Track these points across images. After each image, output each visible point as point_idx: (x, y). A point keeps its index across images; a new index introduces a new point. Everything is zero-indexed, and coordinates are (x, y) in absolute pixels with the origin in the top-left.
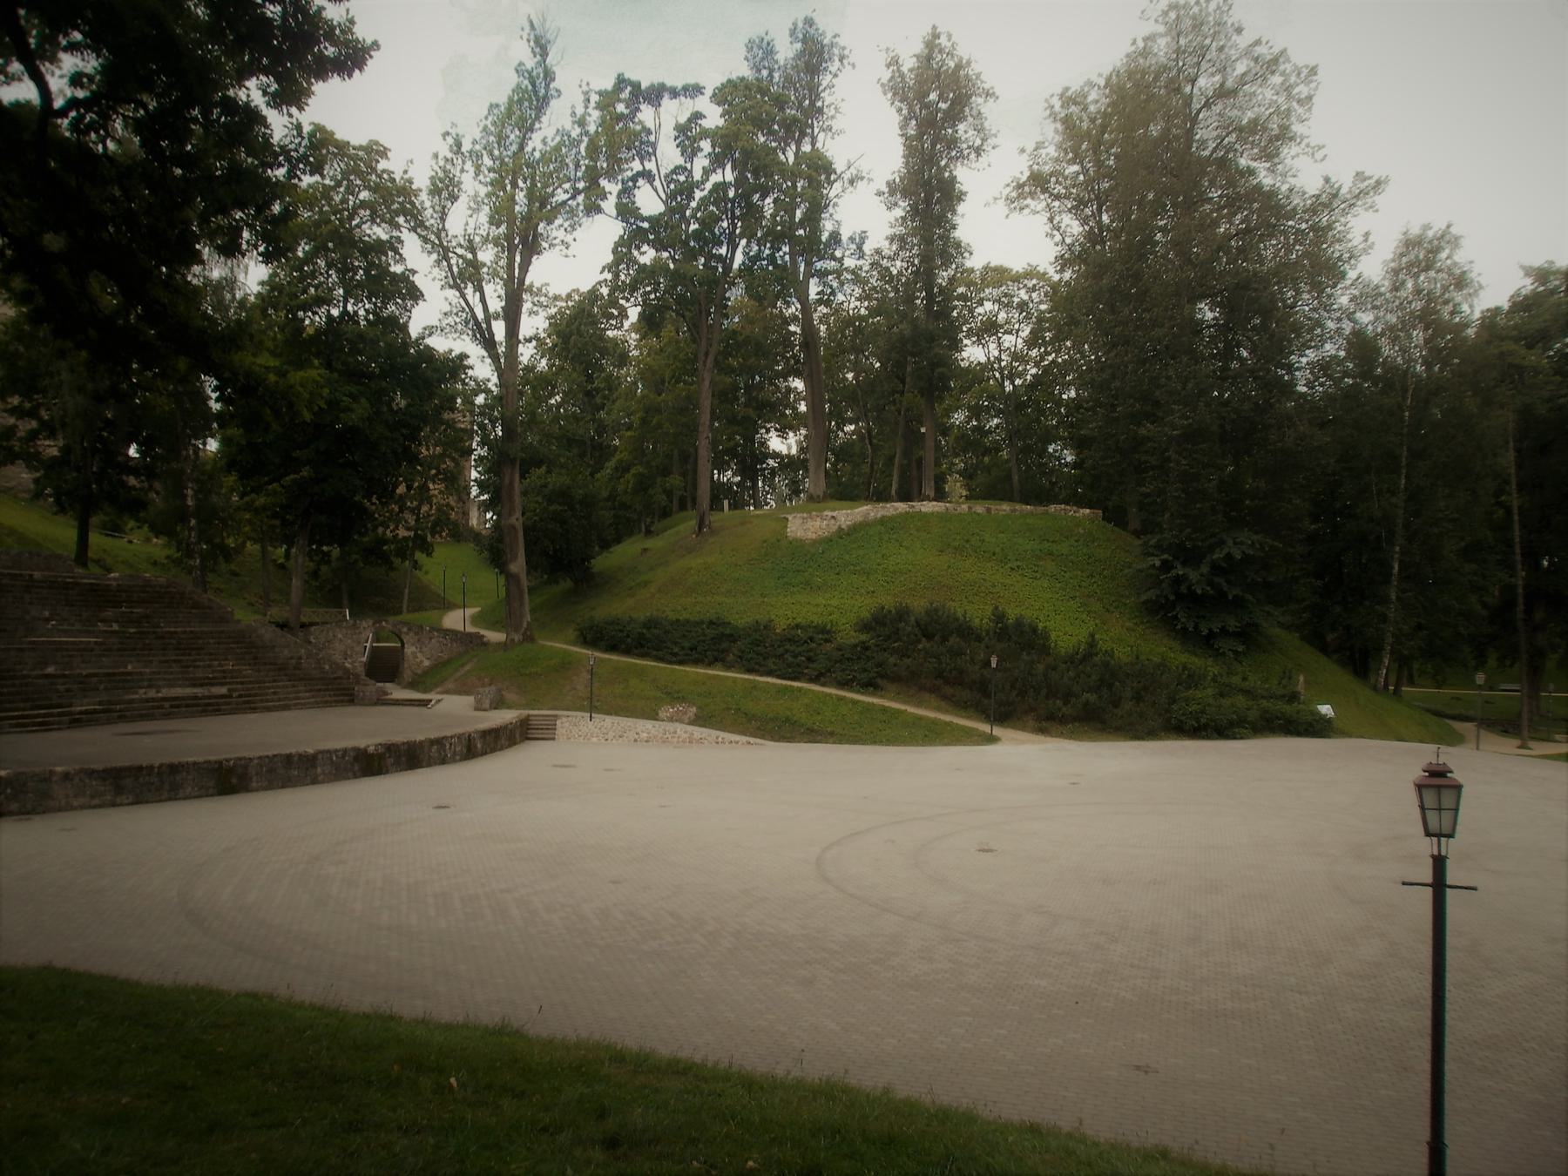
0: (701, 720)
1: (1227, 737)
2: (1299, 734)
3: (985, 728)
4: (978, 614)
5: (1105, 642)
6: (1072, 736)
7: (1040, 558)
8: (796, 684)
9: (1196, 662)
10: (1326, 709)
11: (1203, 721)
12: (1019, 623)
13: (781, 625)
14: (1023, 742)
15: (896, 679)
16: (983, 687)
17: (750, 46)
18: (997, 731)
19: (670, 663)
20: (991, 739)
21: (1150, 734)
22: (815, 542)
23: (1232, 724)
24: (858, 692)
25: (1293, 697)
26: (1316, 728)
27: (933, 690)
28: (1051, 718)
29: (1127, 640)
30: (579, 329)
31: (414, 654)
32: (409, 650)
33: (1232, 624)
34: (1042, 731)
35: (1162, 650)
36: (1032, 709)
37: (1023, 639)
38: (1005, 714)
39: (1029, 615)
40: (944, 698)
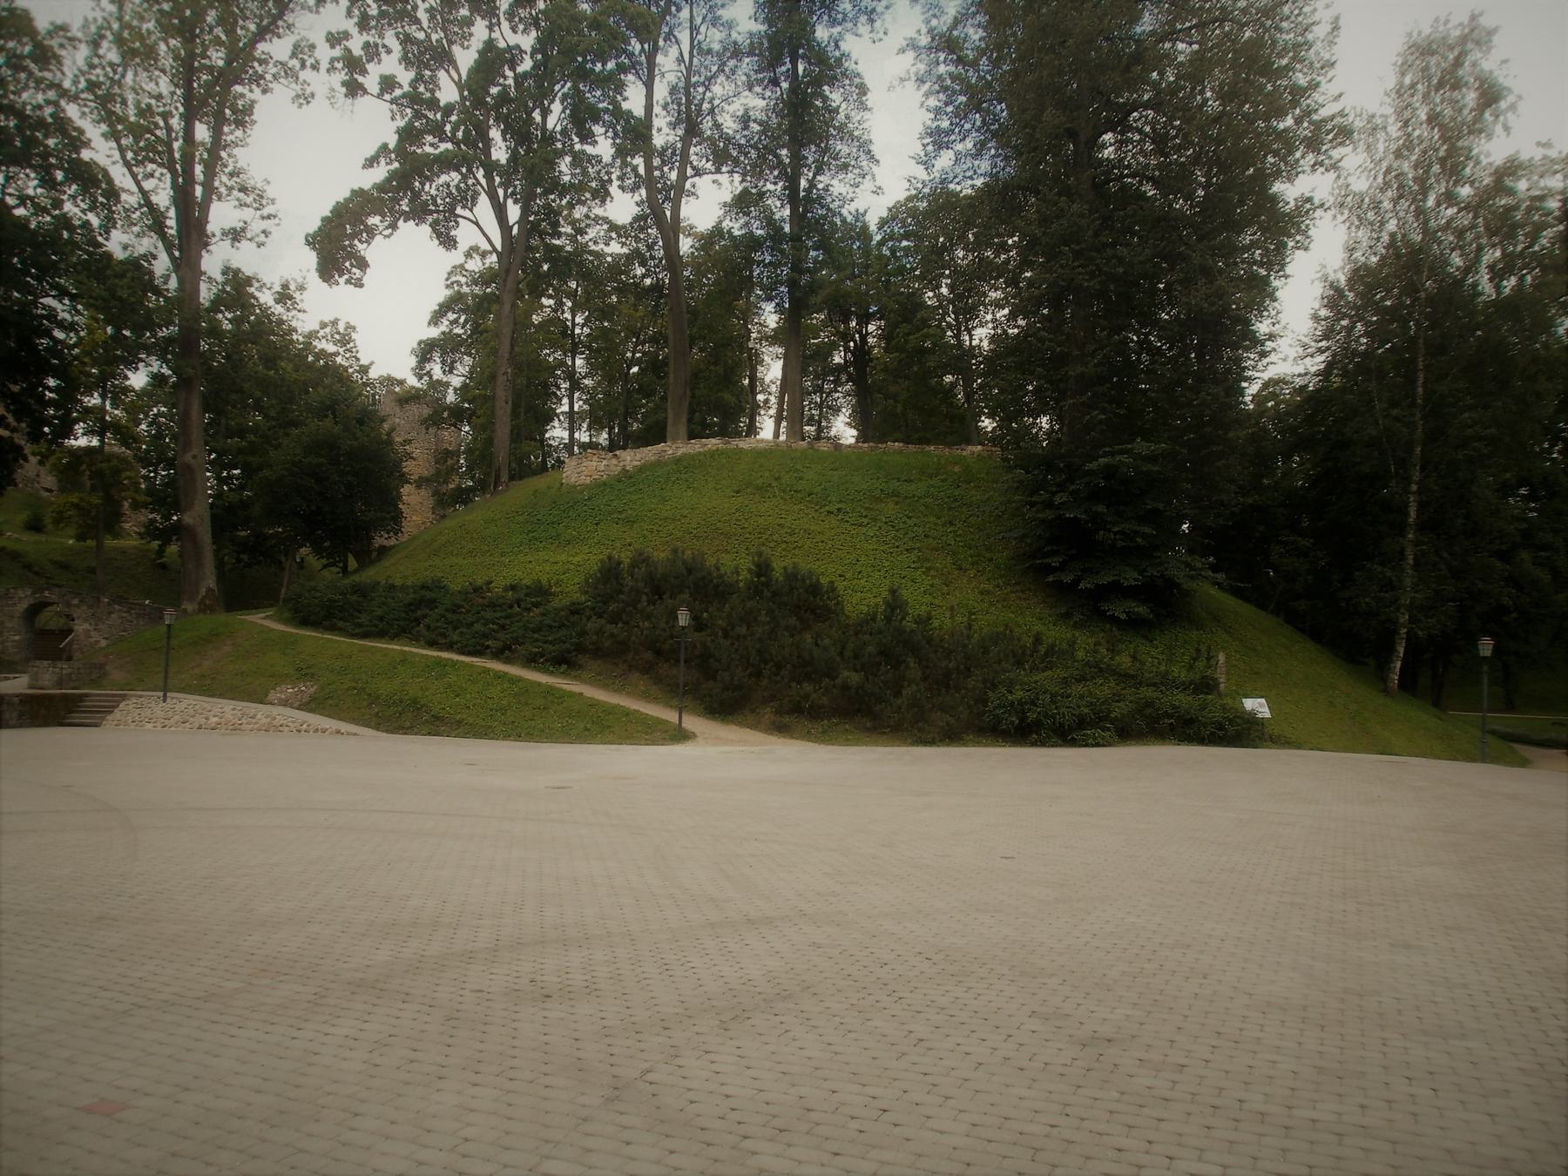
0: (313, 705)
1: (1073, 743)
2: (1202, 741)
3: (671, 716)
4: (735, 564)
5: (917, 600)
6: (824, 737)
7: (879, 500)
8: (445, 655)
9: (1057, 634)
10: (1256, 705)
11: (1031, 716)
12: (792, 576)
13: (499, 584)
14: (726, 742)
15: (597, 653)
16: (704, 663)
17: (308, 243)
18: (691, 722)
19: (353, 636)
20: (680, 735)
21: (951, 736)
22: (585, 487)
23: (1081, 723)
24: (546, 671)
25: (1206, 686)
26: (1238, 732)
27: (647, 669)
28: (797, 709)
29: (960, 600)
30: (599, 255)
31: (87, 633)
32: (81, 627)
33: (1130, 577)
34: (781, 729)
35: (1033, 620)
36: (773, 698)
37: (808, 601)
38: (728, 704)
39: (805, 565)
40: (658, 681)
